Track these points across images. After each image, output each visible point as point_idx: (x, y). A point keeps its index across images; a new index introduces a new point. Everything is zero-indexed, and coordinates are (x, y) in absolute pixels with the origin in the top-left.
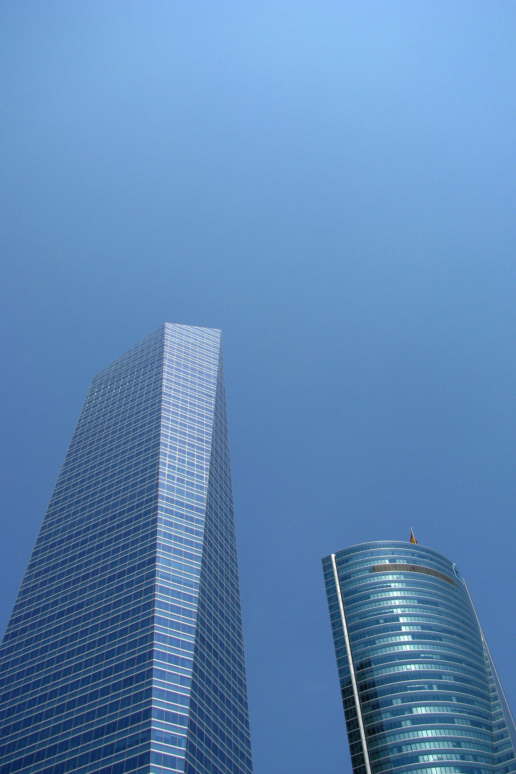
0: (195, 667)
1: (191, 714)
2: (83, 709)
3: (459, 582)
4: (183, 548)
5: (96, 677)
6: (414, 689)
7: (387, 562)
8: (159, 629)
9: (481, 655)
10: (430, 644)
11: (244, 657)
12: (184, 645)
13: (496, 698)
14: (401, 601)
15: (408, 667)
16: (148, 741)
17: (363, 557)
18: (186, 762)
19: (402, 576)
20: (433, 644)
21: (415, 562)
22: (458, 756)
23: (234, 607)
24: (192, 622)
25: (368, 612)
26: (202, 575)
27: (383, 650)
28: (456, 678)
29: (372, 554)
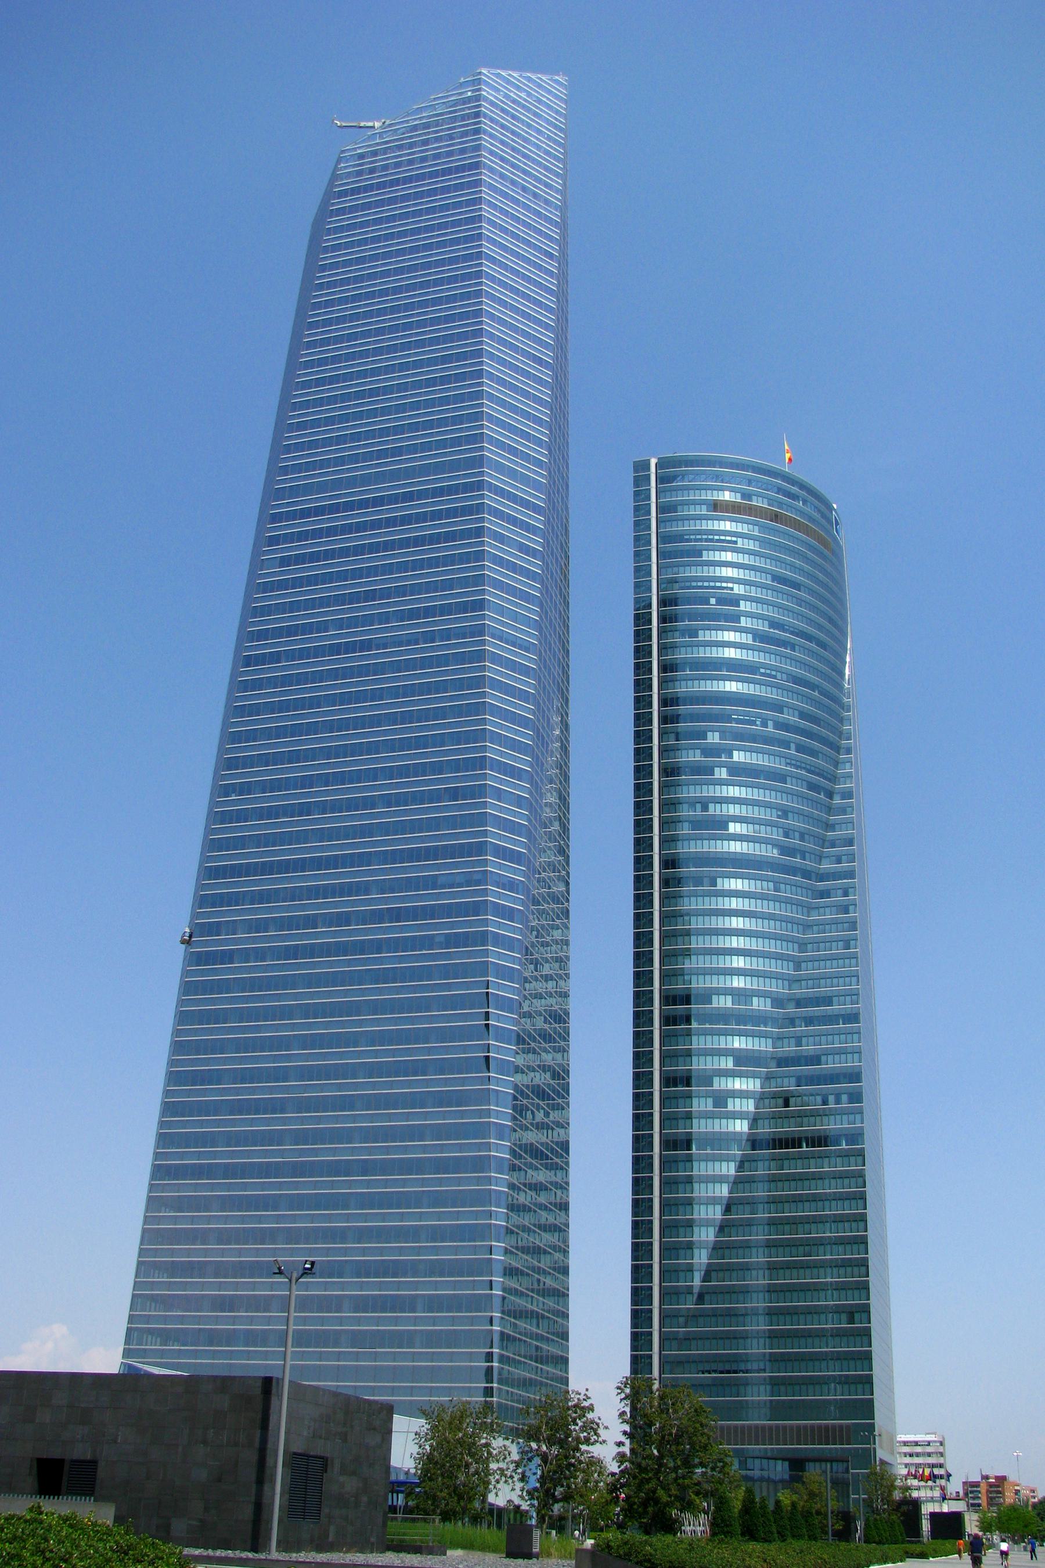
17: (702, 480)
28: (803, 715)
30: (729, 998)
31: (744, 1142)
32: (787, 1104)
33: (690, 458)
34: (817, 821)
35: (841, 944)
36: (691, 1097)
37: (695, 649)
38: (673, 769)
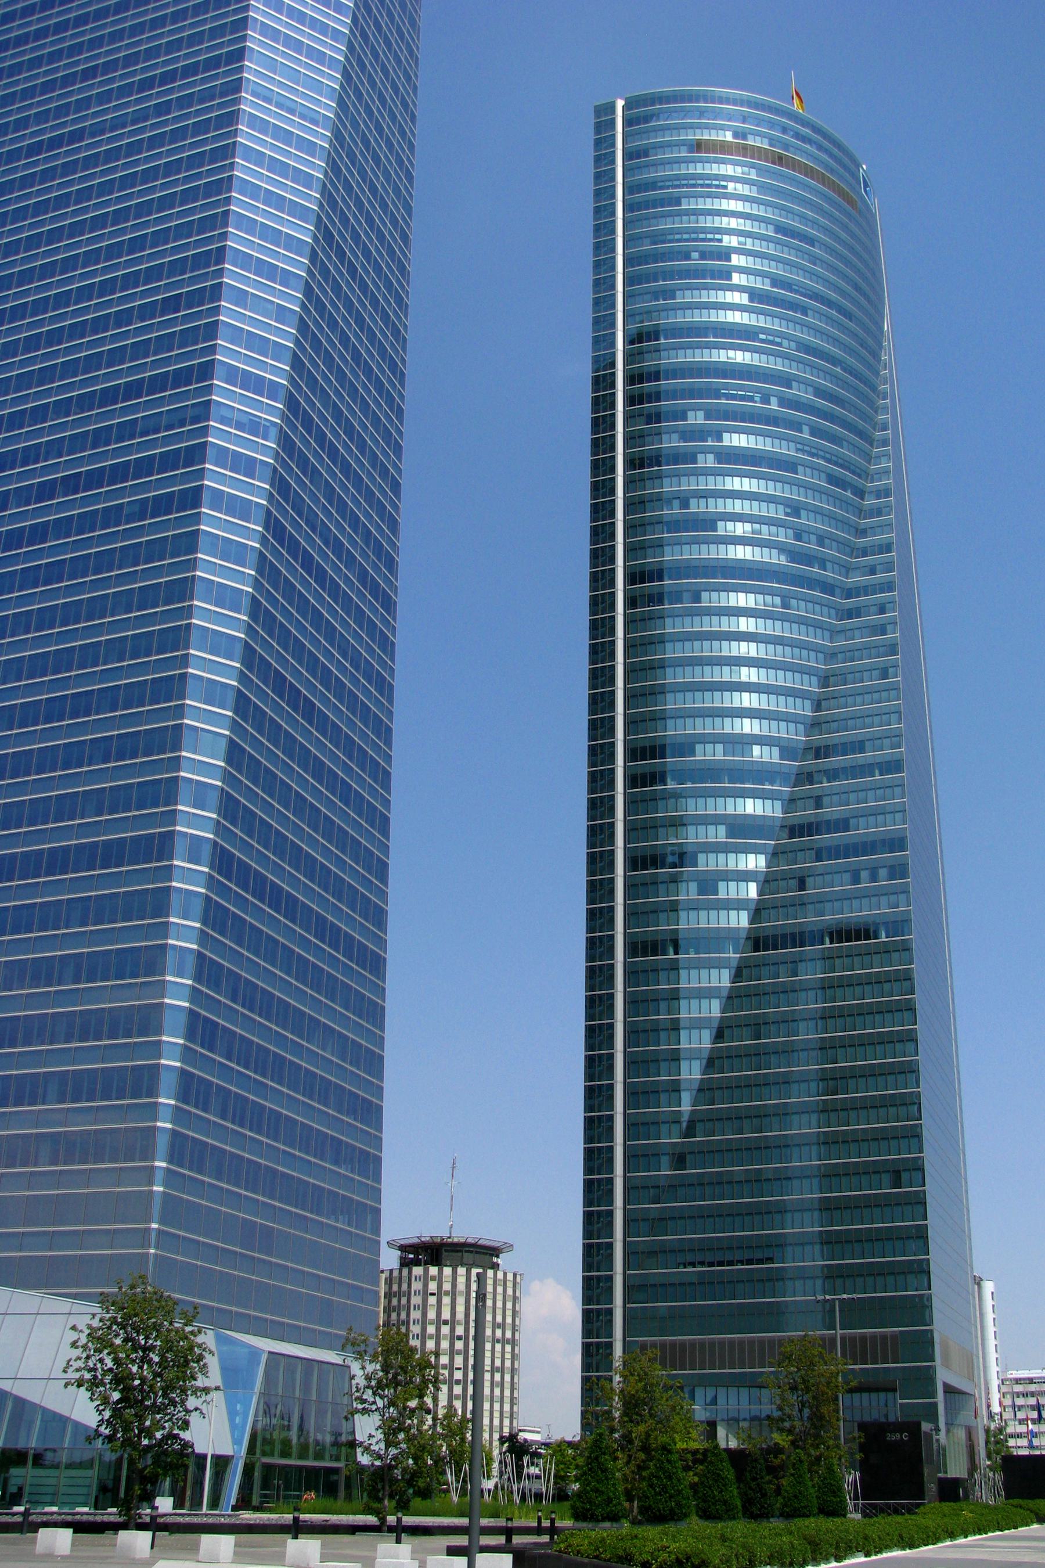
0: (308, 291)
1: (292, 380)
2: (79, 348)
3: (867, 206)
4: (306, 36)
5: (100, 324)
6: (734, 397)
7: (729, 137)
8: (240, 204)
9: (876, 356)
10: (781, 318)
11: (408, 284)
12: (290, 243)
13: (885, 443)
14: (741, 221)
15: (731, 353)
16: (198, 464)
18: (275, 469)
19: (753, 171)
20: (788, 320)
21: (786, 146)
22: (790, 532)
23: (401, 180)
24: (311, 199)
25: (672, 231)
26: (341, 102)
27: (688, 312)
28: (819, 392)
29: (702, 113)
30: (719, 747)
31: (742, 941)
32: (802, 885)
33: (681, 451)
34: (844, 523)
35: (875, 673)
36: (677, 1029)
37: (689, 721)
38: (653, 748)
